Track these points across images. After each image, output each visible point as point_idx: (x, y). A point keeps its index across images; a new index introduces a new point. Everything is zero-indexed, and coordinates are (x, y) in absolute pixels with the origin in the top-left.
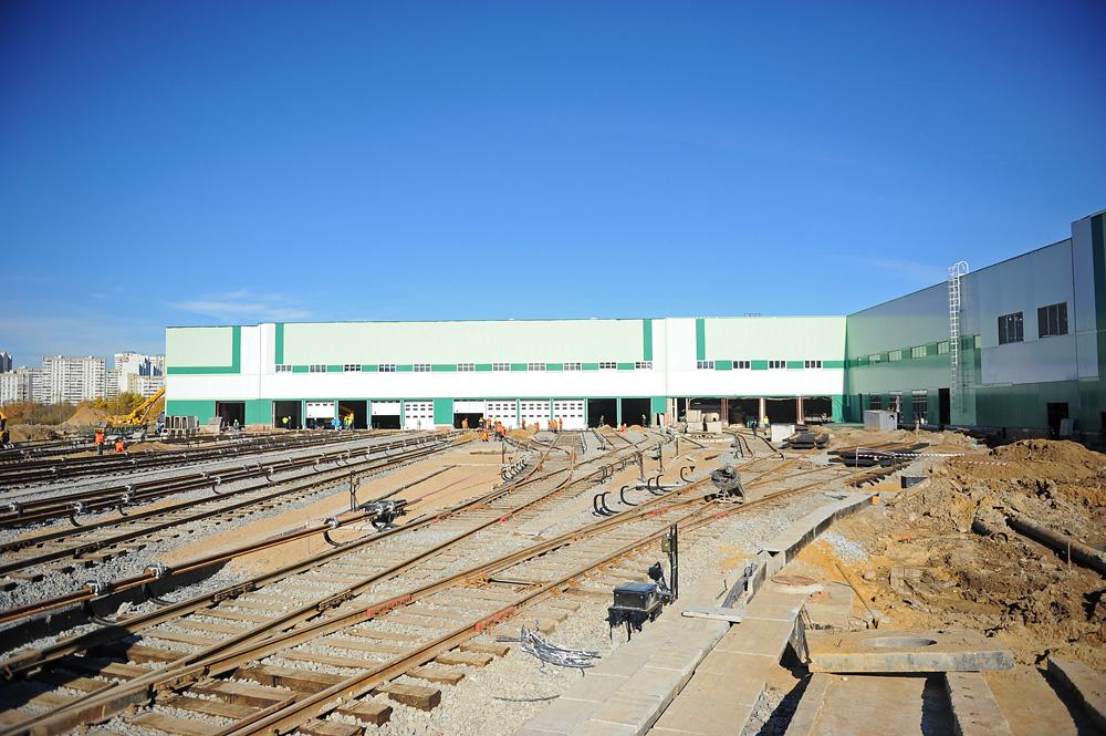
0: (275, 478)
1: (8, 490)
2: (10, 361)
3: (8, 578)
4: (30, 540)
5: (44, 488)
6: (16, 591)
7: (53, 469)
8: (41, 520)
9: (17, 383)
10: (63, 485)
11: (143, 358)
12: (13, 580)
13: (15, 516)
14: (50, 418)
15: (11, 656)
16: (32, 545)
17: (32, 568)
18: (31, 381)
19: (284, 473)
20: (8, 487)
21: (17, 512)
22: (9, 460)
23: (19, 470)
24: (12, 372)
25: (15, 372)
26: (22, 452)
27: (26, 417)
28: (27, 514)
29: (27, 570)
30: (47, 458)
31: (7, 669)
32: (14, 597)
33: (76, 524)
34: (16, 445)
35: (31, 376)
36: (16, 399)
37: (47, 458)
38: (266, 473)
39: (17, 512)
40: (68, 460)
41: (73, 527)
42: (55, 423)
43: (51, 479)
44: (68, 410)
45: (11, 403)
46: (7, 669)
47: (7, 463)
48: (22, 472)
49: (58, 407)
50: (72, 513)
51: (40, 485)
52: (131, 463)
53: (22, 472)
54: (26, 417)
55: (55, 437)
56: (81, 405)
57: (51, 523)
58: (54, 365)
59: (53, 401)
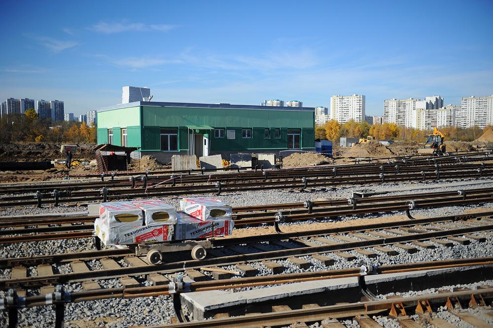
0: (419, 215)
1: (451, 182)
2: (442, 101)
3: (464, 237)
4: (474, 215)
5: (472, 182)
6: (470, 246)
7: (478, 170)
8: (476, 203)
9: (446, 115)
10: (484, 181)
11: (435, 97)
12: (467, 239)
13: (351, 208)
14: (466, 137)
15: (479, 288)
16: (475, 218)
17: (478, 233)
18: (454, 113)
19: (449, 209)
20: (451, 180)
21: (353, 205)
22: (448, 163)
23: (455, 170)
24: (443, 108)
25: (445, 108)
26: (455, 158)
27: (452, 136)
28: (359, 207)
29: (475, 233)
30: (470, 163)
31: (481, 296)
32: (469, 250)
33: (410, 217)
34: (450, 153)
35: (455, 110)
36: (445, 125)
37: (470, 163)
38: (404, 208)
39: (353, 205)
40: (486, 165)
41: (409, 219)
42: (470, 141)
43: (477, 176)
44: (477, 132)
45: (443, 127)
46: (481, 296)
47: (447, 164)
48: (457, 171)
49: (471, 130)
50: (407, 210)
51: (470, 180)
52: (434, 174)
53: (457, 171)
54: (452, 136)
55: (472, 149)
56: (487, 129)
57: (482, 205)
58: (469, 102)
59: (468, 127)
